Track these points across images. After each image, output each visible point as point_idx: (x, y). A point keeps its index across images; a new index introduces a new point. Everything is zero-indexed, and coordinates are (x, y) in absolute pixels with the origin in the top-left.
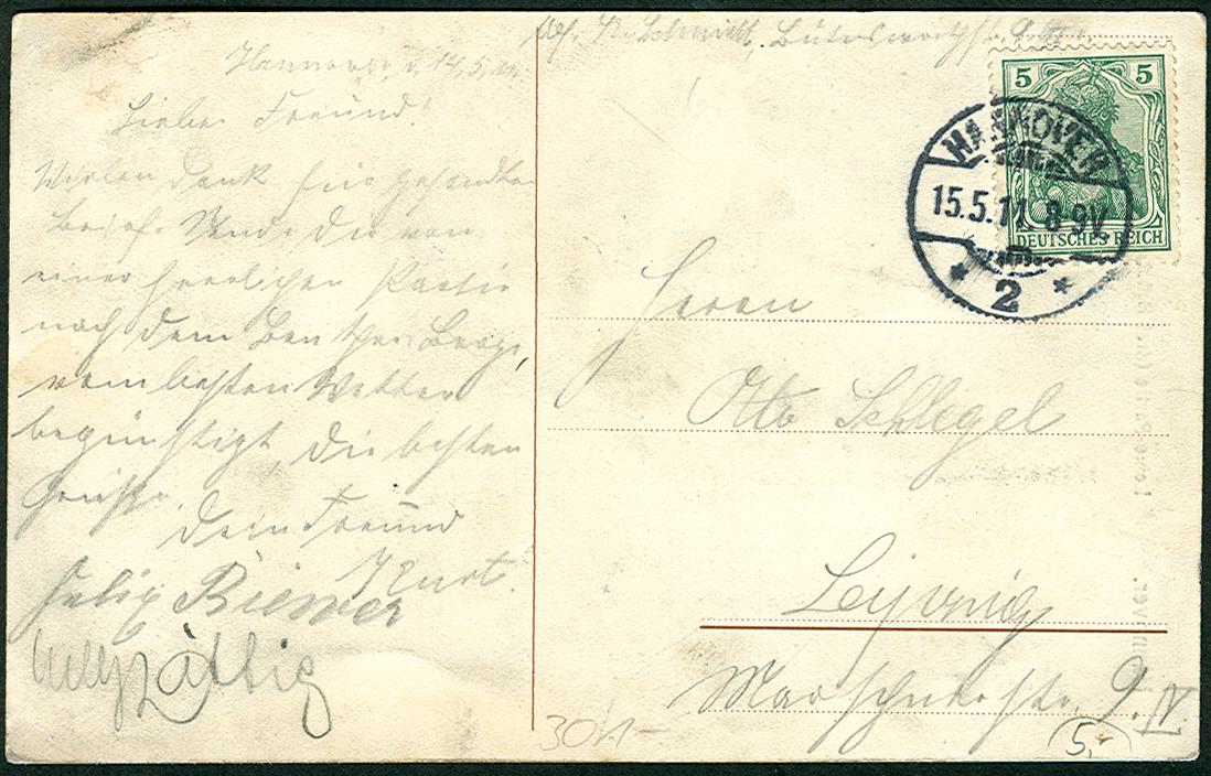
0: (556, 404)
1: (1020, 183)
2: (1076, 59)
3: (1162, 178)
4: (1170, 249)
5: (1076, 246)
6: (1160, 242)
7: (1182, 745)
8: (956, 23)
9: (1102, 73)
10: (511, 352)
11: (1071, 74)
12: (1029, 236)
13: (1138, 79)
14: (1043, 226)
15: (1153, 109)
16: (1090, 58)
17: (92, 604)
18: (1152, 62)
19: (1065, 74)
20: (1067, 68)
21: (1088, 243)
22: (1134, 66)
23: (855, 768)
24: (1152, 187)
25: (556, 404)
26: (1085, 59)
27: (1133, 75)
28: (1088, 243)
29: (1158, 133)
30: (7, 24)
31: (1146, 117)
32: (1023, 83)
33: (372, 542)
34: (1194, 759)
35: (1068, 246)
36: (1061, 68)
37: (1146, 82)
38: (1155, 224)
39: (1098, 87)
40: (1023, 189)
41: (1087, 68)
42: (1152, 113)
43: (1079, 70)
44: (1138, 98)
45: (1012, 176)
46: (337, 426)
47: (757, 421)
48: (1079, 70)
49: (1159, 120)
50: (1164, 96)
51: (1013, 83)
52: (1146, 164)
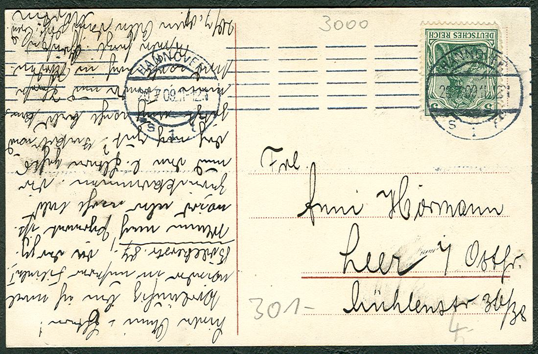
4: (426, 29)
5: (468, 32)
12: (444, 37)
28: (446, 33)
31: (434, 89)
42: (431, 90)
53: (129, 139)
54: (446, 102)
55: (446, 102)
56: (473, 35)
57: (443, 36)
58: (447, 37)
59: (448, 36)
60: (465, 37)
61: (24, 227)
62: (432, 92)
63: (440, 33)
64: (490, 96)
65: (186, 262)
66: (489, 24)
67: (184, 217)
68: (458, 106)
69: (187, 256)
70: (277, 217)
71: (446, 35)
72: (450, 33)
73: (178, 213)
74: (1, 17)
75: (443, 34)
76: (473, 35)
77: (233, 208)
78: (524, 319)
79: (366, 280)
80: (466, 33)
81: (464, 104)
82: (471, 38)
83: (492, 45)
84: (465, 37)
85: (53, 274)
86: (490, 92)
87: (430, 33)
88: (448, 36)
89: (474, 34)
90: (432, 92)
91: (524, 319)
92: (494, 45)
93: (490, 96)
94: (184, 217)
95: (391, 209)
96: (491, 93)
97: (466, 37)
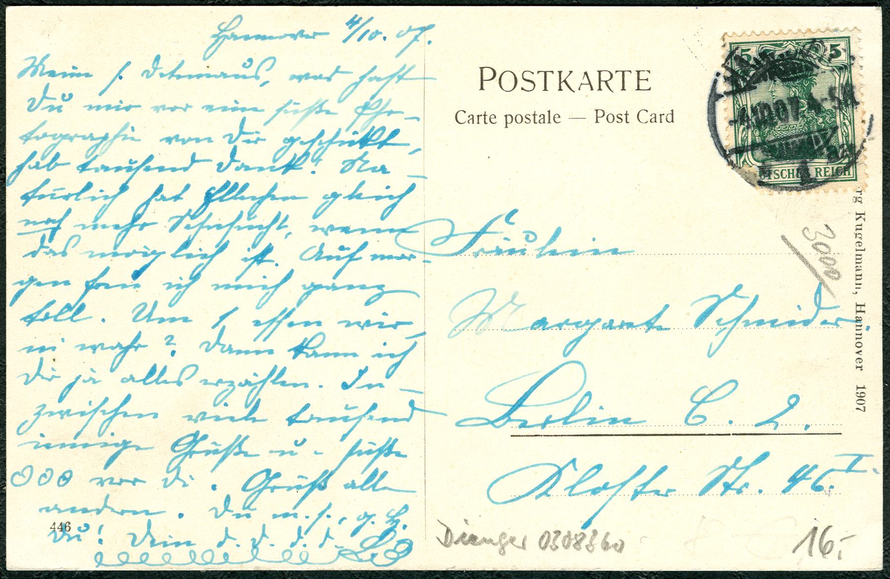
0: (485, 122)
1: (744, 133)
2: (784, 41)
3: (849, 127)
4: (856, 180)
5: (786, 179)
6: (849, 174)
8: (301, 479)
10: (377, 146)
12: (825, 168)
16: (795, 40)
23: (886, 488)
24: (843, 134)
25: (485, 122)
26: (791, 41)
30: (157, 574)
33: (254, 222)
35: (781, 179)
40: (747, 137)
42: (842, 79)
45: (738, 130)
52: (838, 118)
53: (31, 466)
56: (777, 174)
57: (827, 169)
58: (821, 170)
60: (791, 172)
61: (30, 167)
62: (840, 77)
65: (342, 171)
66: (836, 30)
67: (23, 205)
76: (777, 174)
78: (97, 567)
80: (789, 177)
82: (780, 170)
83: (745, 161)
84: (791, 172)
85: (490, 398)
87: (849, 174)
88: (819, 170)
89: (777, 177)
90: (840, 77)
91: (97, 567)
92: (742, 160)
94: (23, 205)
95: (452, 238)
97: (789, 170)
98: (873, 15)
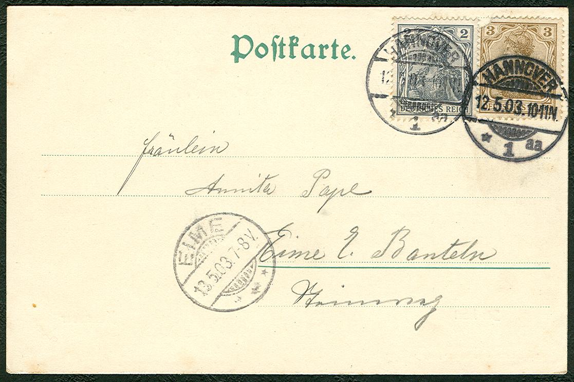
2: (516, 23)
7: (560, 367)
9: (527, 30)
11: (512, 30)
12: (452, 107)
13: (545, 34)
14: (494, 100)
15: (551, 48)
17: (315, 305)
18: (551, 27)
19: (510, 30)
20: (511, 27)
21: (451, 111)
22: (459, 30)
26: (437, 25)
27: (543, 32)
28: (451, 111)
29: (552, 60)
31: (547, 52)
32: (490, 33)
34: (565, 373)
36: (509, 27)
37: (492, 34)
38: (549, 102)
39: (525, 37)
41: (521, 28)
42: (550, 50)
43: (517, 28)
44: (544, 43)
46: (321, 194)
47: (341, 193)
48: (517, 28)
49: (553, 54)
50: (473, 44)
51: (486, 33)
52: (463, 75)
54: (536, 38)
55: (536, 38)
59: (448, 108)
63: (457, 112)
64: (488, 43)
68: (522, 33)
69: (354, 233)
70: (128, 196)
71: (451, 110)
72: (447, 111)
73: (527, 163)
74: (3, 238)
75: (454, 111)
77: (388, 119)
79: (472, 372)
81: (516, 35)
86: (488, 47)
88: (448, 108)
93: (488, 43)
96: (487, 47)
98: (561, 14)
